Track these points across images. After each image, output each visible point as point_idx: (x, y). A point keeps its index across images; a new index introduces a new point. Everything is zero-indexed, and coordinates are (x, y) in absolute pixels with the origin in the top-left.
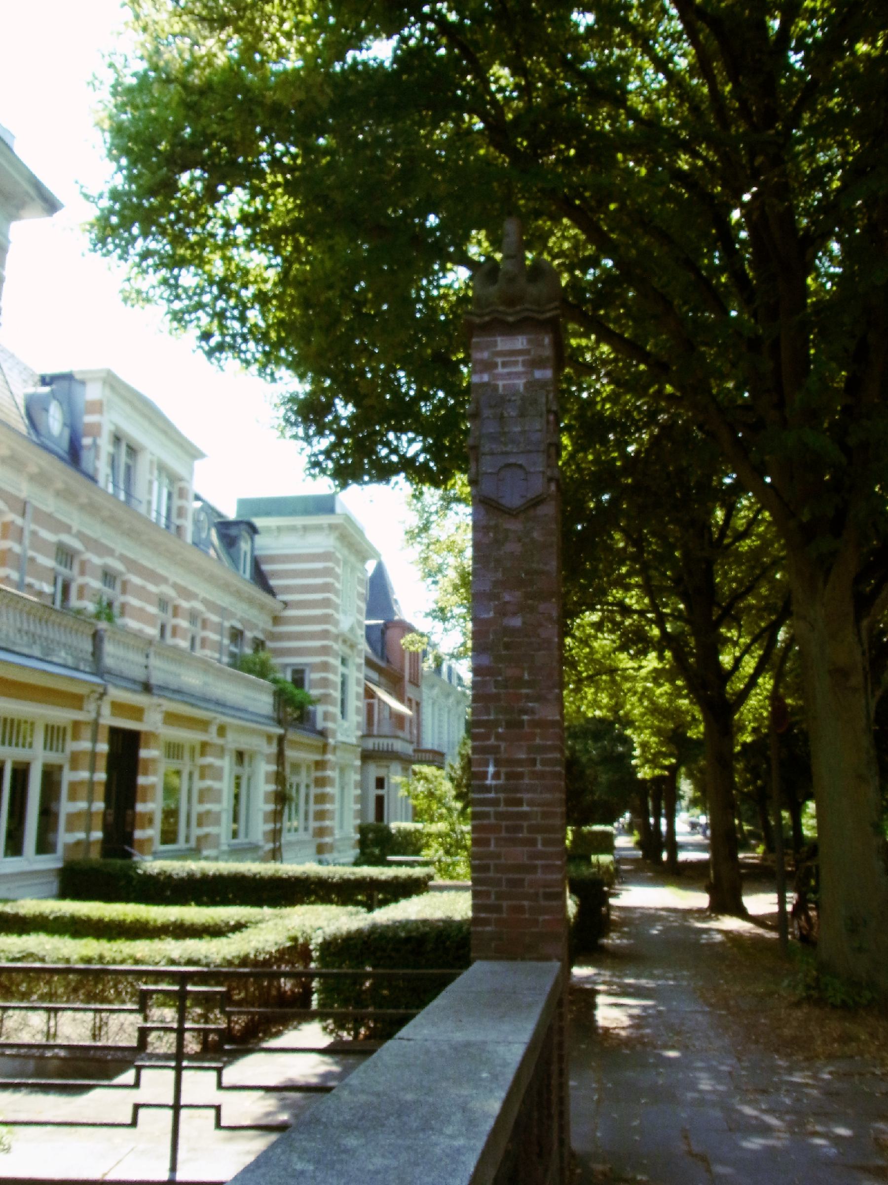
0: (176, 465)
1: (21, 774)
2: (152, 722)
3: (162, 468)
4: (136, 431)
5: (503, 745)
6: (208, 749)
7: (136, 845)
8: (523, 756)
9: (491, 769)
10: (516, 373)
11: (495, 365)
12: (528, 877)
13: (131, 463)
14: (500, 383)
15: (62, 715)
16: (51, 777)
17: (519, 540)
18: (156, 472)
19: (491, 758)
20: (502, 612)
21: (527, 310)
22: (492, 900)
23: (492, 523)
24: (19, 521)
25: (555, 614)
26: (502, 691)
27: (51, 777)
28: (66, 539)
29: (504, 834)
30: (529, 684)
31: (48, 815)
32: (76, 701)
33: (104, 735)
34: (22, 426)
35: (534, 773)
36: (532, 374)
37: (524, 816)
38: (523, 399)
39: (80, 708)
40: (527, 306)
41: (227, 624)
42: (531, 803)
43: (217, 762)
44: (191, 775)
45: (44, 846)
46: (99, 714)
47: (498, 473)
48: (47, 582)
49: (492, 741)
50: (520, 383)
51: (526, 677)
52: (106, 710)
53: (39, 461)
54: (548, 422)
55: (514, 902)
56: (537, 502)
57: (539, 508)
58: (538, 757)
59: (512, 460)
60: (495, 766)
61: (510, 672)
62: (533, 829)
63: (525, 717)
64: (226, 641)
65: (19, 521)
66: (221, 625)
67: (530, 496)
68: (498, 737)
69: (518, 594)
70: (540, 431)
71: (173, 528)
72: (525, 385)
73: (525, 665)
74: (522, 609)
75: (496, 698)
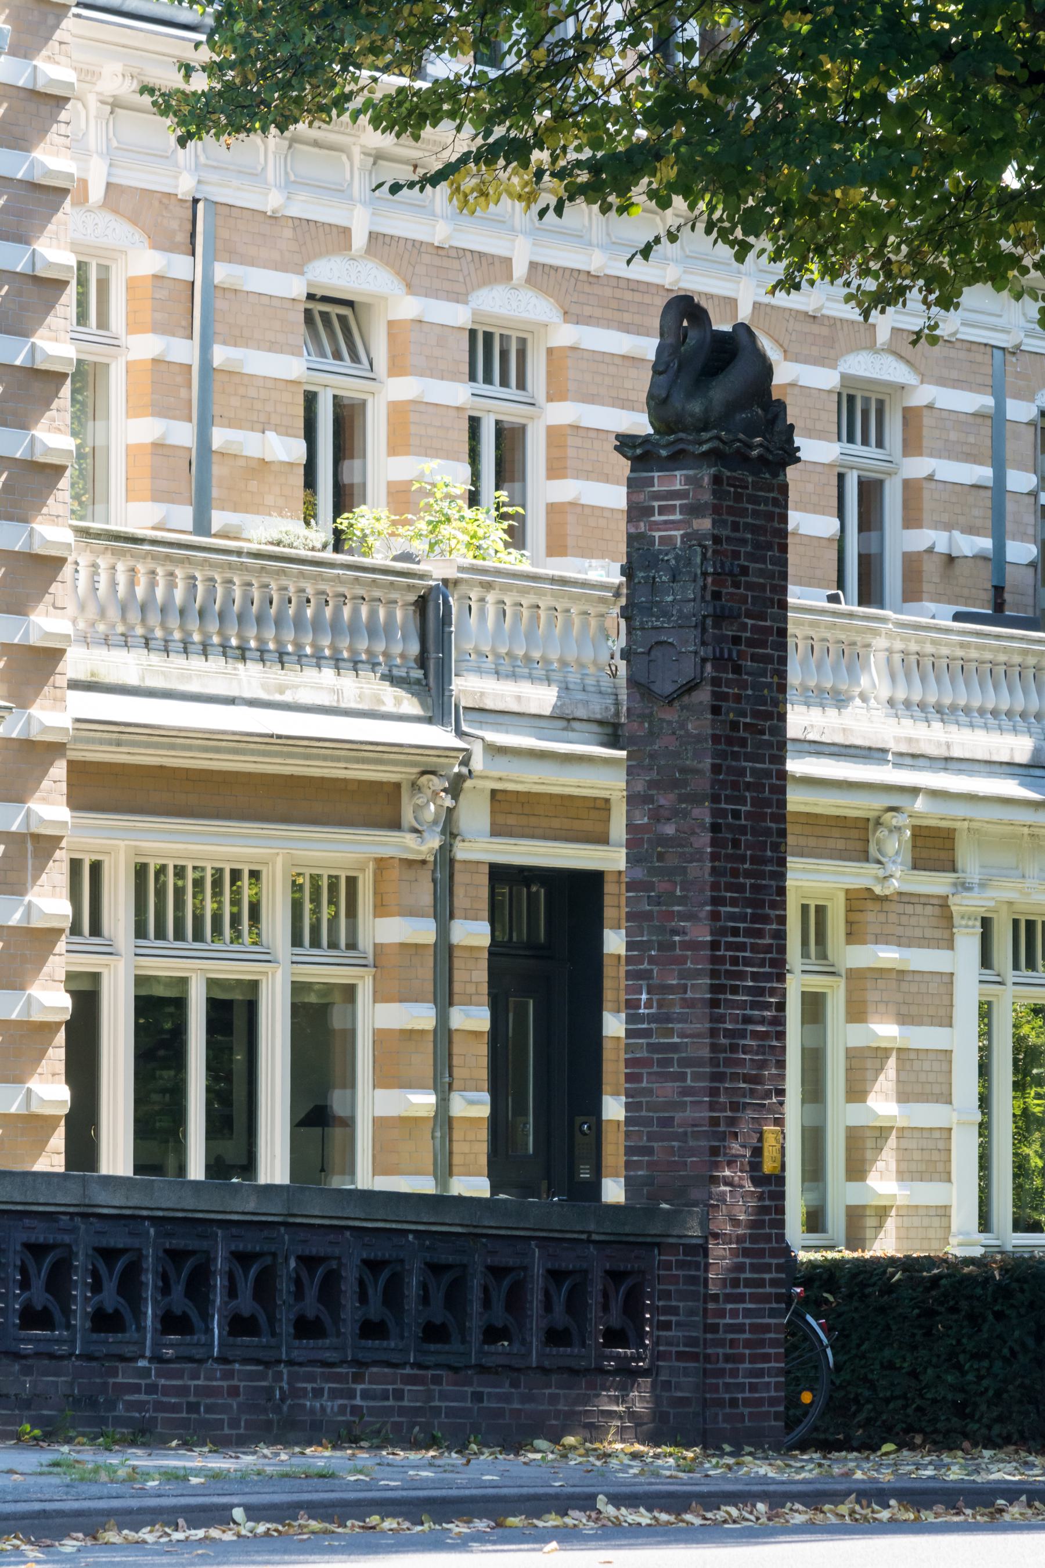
1: (233, 1016)
5: (656, 969)
6: (871, 916)
9: (644, 997)
12: (678, 1116)
14: (657, 534)
16: (319, 1024)
17: (674, 733)
20: (656, 817)
21: (681, 440)
22: (644, 1142)
23: (647, 711)
25: (708, 820)
27: (319, 1024)
28: (334, 275)
29: (655, 1069)
30: (682, 900)
33: (473, 891)
37: (674, 1048)
38: (677, 558)
39: (395, 825)
42: (682, 1035)
46: (450, 832)
47: (649, 652)
48: (284, 431)
49: (645, 966)
51: (678, 893)
52: (474, 815)
54: (704, 588)
55: (665, 1144)
56: (690, 687)
57: (694, 694)
59: (663, 638)
60: (648, 993)
61: (662, 886)
62: (684, 1062)
63: (677, 938)
66: (997, 419)
67: (682, 681)
68: (652, 960)
69: (672, 796)
70: (694, 600)
72: (682, 536)
73: (678, 879)
74: (675, 813)
75: (647, 916)
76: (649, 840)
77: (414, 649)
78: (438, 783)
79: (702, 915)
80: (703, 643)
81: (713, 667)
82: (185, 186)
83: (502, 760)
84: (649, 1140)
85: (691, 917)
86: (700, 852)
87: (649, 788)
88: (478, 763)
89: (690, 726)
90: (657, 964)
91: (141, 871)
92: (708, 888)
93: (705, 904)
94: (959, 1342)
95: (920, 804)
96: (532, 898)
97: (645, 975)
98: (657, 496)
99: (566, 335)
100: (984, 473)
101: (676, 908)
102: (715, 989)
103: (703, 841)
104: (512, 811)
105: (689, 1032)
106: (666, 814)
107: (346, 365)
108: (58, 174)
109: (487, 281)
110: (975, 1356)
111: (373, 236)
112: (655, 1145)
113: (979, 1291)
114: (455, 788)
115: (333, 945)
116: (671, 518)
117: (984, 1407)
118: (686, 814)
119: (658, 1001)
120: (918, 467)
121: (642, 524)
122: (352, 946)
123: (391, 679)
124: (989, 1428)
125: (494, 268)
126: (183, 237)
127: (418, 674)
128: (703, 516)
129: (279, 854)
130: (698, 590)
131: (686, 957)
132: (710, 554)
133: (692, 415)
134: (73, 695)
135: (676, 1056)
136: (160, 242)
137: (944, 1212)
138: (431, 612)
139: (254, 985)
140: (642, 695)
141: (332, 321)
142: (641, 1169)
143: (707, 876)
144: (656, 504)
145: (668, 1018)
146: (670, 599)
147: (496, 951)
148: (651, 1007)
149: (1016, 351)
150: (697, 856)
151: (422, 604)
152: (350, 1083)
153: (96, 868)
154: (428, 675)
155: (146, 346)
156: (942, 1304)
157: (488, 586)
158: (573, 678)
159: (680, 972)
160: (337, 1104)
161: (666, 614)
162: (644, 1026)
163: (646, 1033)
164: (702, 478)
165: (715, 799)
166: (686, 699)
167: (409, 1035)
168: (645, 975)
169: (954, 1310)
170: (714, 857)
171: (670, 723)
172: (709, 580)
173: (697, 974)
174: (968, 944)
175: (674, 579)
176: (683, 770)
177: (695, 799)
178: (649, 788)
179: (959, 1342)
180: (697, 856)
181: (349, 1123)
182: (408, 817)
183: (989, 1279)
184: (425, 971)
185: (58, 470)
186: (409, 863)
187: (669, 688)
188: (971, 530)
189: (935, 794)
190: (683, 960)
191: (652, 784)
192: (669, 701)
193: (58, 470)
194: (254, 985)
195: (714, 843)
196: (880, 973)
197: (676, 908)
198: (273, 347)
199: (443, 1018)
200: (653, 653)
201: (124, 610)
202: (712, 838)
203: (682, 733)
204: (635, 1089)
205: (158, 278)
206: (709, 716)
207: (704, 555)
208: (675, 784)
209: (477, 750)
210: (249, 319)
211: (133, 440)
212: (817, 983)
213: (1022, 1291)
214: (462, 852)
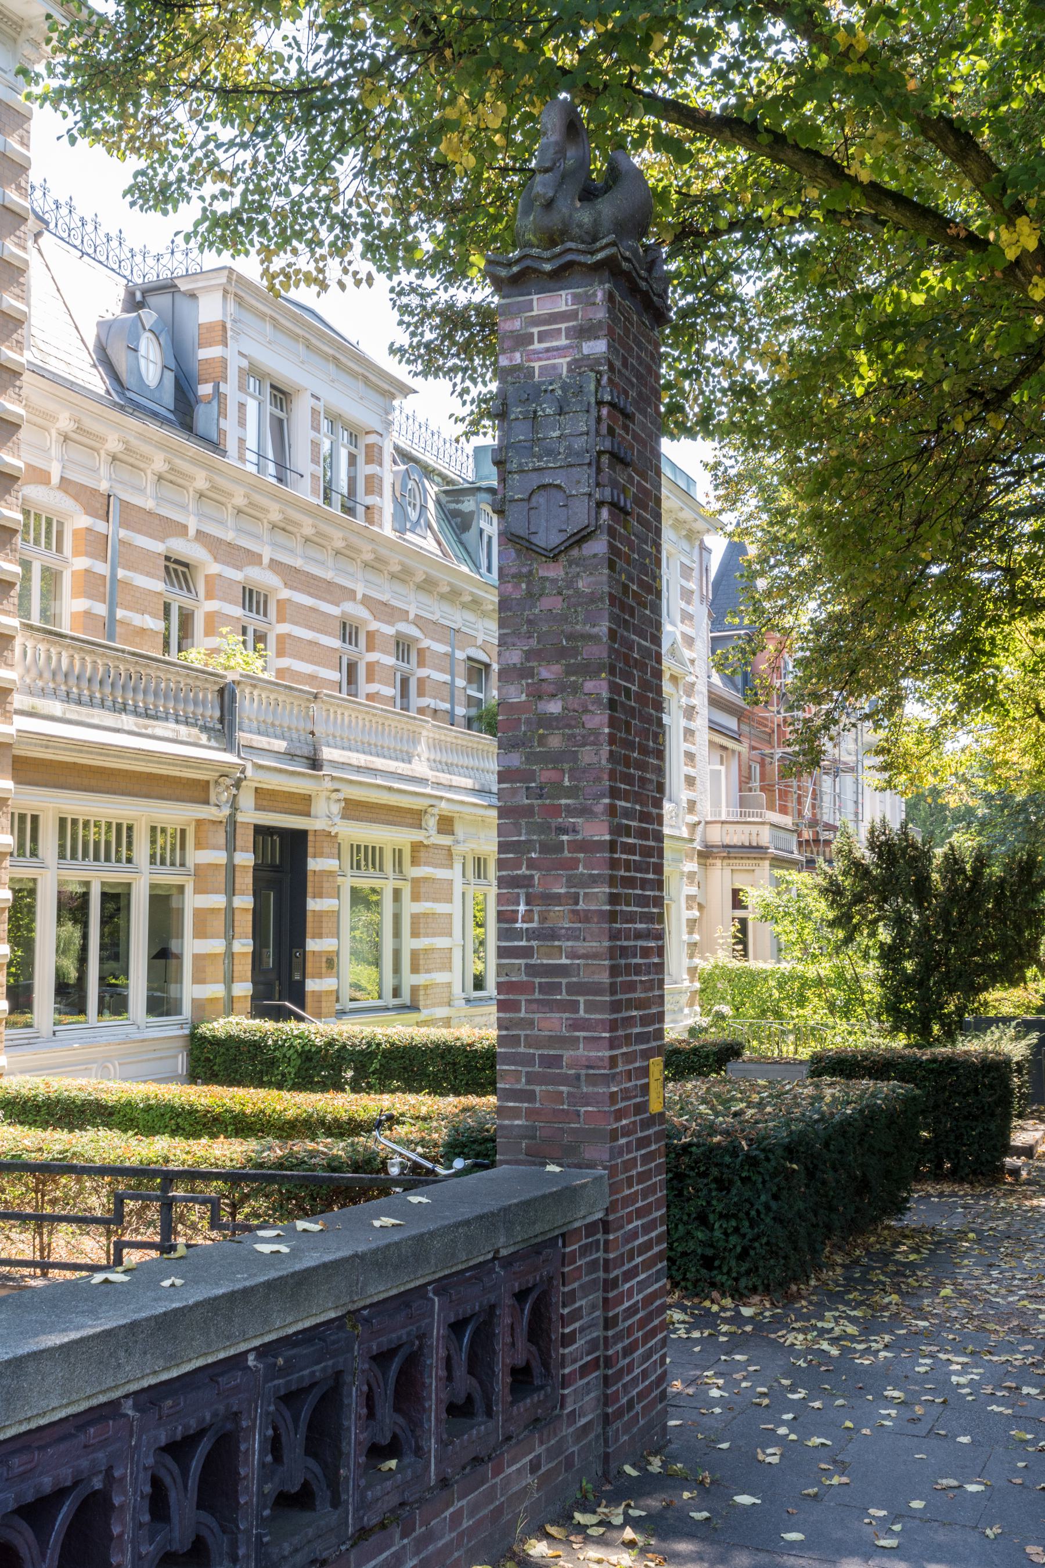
0: (359, 410)
1: (116, 902)
2: (323, 818)
3: (335, 419)
4: (285, 365)
6: (422, 854)
7: (309, 1000)
8: (563, 891)
9: (522, 908)
10: (557, 349)
11: (528, 339)
12: (567, 1054)
13: (282, 415)
14: (536, 365)
15: (400, 837)
17: (560, 594)
18: (325, 425)
19: (522, 891)
20: (537, 694)
23: (524, 570)
24: (100, 526)
25: (605, 695)
26: (536, 802)
27: (164, 906)
29: (537, 996)
30: (572, 792)
31: (163, 955)
32: (196, 791)
33: (245, 838)
34: (96, 382)
35: (575, 912)
36: (579, 348)
38: (564, 387)
39: (206, 802)
40: (571, 245)
41: (460, 655)
42: (572, 955)
43: (441, 873)
44: (397, 894)
45: (160, 1005)
46: (235, 808)
48: (154, 616)
49: (523, 871)
50: (562, 362)
51: (567, 783)
52: (247, 800)
53: (121, 431)
54: (599, 419)
55: (550, 1088)
56: (582, 537)
58: (582, 892)
59: (547, 481)
60: (527, 904)
61: (546, 775)
62: (572, 989)
63: (565, 838)
64: (461, 683)
65: (100, 526)
66: (451, 656)
67: (571, 529)
68: (531, 864)
69: (557, 668)
71: (360, 510)
72: (569, 364)
73: (566, 766)
74: (561, 689)
76: (528, 721)
77: (217, 714)
78: (229, 781)
79: (599, 808)
80: (598, 485)
81: (610, 513)
82: (104, 486)
83: (261, 772)
84: (528, 1082)
85: (585, 811)
86: (595, 732)
87: (528, 659)
88: (249, 772)
89: (580, 584)
90: (539, 869)
91: (62, 821)
92: (606, 777)
93: (603, 796)
94: (709, 1203)
95: (443, 804)
96: (273, 842)
97: (523, 882)
98: (537, 321)
99: (285, 594)
100: (447, 678)
101: (563, 802)
102: (614, 899)
103: (599, 720)
104: (265, 798)
105: (582, 951)
106: (551, 689)
107: (185, 593)
108: (14, 413)
109: (250, 563)
110: (721, 1216)
111: (199, 532)
112: (537, 1089)
113: (728, 1159)
114: (237, 785)
115: (173, 864)
116: (555, 344)
117: (733, 1263)
118: (576, 689)
119: (540, 913)
120: (423, 672)
121: (518, 355)
122: (183, 865)
123: (204, 729)
124: (736, 1280)
125: (255, 559)
126: (102, 512)
127: (219, 726)
128: (597, 338)
129: (140, 812)
130: (592, 423)
131: (577, 861)
132: (604, 381)
133: (580, 226)
134: (16, 718)
135: (564, 981)
136: (90, 512)
137: (449, 985)
138: (226, 696)
139: (129, 885)
140: (518, 552)
141: (178, 571)
142: (518, 1118)
143: (604, 762)
144: (535, 330)
145: (552, 935)
146: (557, 433)
147: (256, 868)
148: (531, 921)
149: (458, 631)
150: (591, 738)
151: (221, 691)
152: (181, 936)
153: (35, 819)
154: (224, 726)
155: (81, 563)
156: (692, 1169)
157: (254, 686)
158: (295, 736)
159: (569, 879)
160: (174, 947)
161: (550, 453)
162: (523, 943)
163: (526, 952)
164: (595, 295)
165: (612, 671)
166: (575, 552)
167: (213, 911)
168: (523, 882)
169: (704, 1175)
170: (612, 740)
171: (554, 581)
172: (605, 411)
173: (594, 880)
174: (458, 867)
175: (561, 412)
176: (570, 637)
177: (589, 670)
178: (528, 659)
179: (709, 1203)
180: (591, 738)
181: (179, 957)
182: (213, 798)
183: (734, 1150)
184: (221, 877)
185: (11, 585)
186: (214, 822)
187: (555, 539)
188: (443, 700)
189: (449, 800)
190: (573, 864)
191: (529, 655)
192: (554, 555)
193: (11, 585)
194: (129, 885)
195: (612, 723)
196: (425, 879)
197: (563, 802)
198: (148, 574)
199: (230, 902)
200: (534, 499)
201: (54, 674)
202: (611, 717)
203: (571, 592)
204: (511, 1020)
205: (89, 530)
206: (606, 571)
207: (598, 381)
208: (562, 653)
209: (249, 766)
210: (136, 559)
211: (75, 609)
212: (399, 884)
213: (768, 1159)
214: (240, 818)
